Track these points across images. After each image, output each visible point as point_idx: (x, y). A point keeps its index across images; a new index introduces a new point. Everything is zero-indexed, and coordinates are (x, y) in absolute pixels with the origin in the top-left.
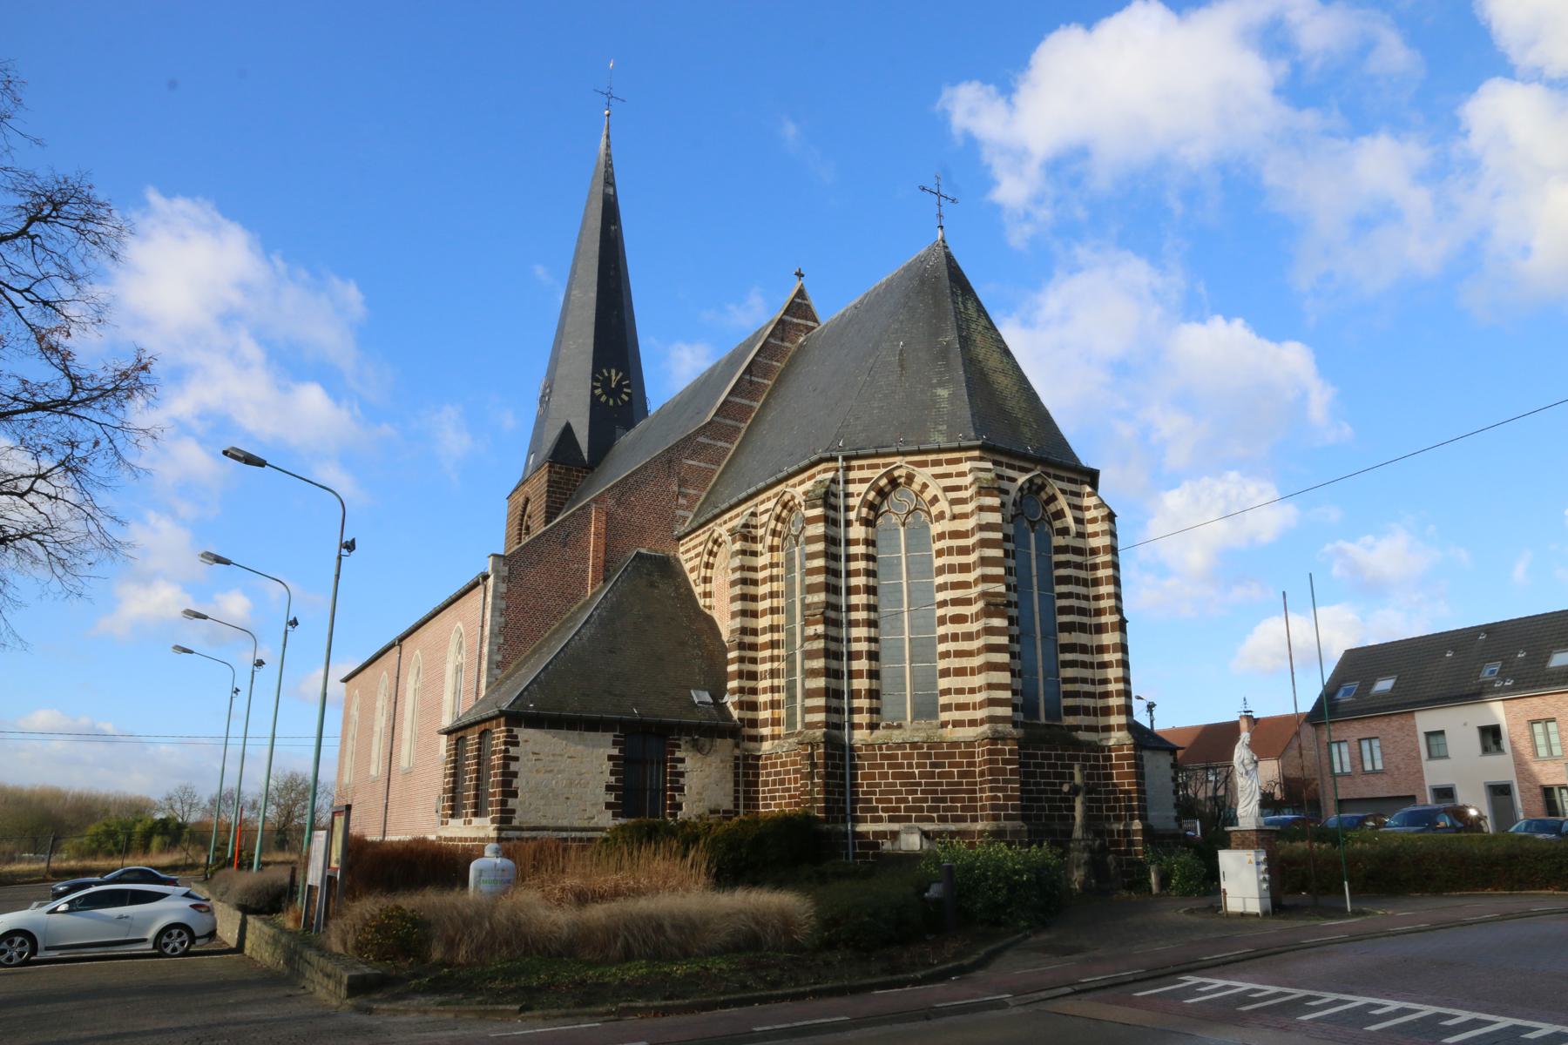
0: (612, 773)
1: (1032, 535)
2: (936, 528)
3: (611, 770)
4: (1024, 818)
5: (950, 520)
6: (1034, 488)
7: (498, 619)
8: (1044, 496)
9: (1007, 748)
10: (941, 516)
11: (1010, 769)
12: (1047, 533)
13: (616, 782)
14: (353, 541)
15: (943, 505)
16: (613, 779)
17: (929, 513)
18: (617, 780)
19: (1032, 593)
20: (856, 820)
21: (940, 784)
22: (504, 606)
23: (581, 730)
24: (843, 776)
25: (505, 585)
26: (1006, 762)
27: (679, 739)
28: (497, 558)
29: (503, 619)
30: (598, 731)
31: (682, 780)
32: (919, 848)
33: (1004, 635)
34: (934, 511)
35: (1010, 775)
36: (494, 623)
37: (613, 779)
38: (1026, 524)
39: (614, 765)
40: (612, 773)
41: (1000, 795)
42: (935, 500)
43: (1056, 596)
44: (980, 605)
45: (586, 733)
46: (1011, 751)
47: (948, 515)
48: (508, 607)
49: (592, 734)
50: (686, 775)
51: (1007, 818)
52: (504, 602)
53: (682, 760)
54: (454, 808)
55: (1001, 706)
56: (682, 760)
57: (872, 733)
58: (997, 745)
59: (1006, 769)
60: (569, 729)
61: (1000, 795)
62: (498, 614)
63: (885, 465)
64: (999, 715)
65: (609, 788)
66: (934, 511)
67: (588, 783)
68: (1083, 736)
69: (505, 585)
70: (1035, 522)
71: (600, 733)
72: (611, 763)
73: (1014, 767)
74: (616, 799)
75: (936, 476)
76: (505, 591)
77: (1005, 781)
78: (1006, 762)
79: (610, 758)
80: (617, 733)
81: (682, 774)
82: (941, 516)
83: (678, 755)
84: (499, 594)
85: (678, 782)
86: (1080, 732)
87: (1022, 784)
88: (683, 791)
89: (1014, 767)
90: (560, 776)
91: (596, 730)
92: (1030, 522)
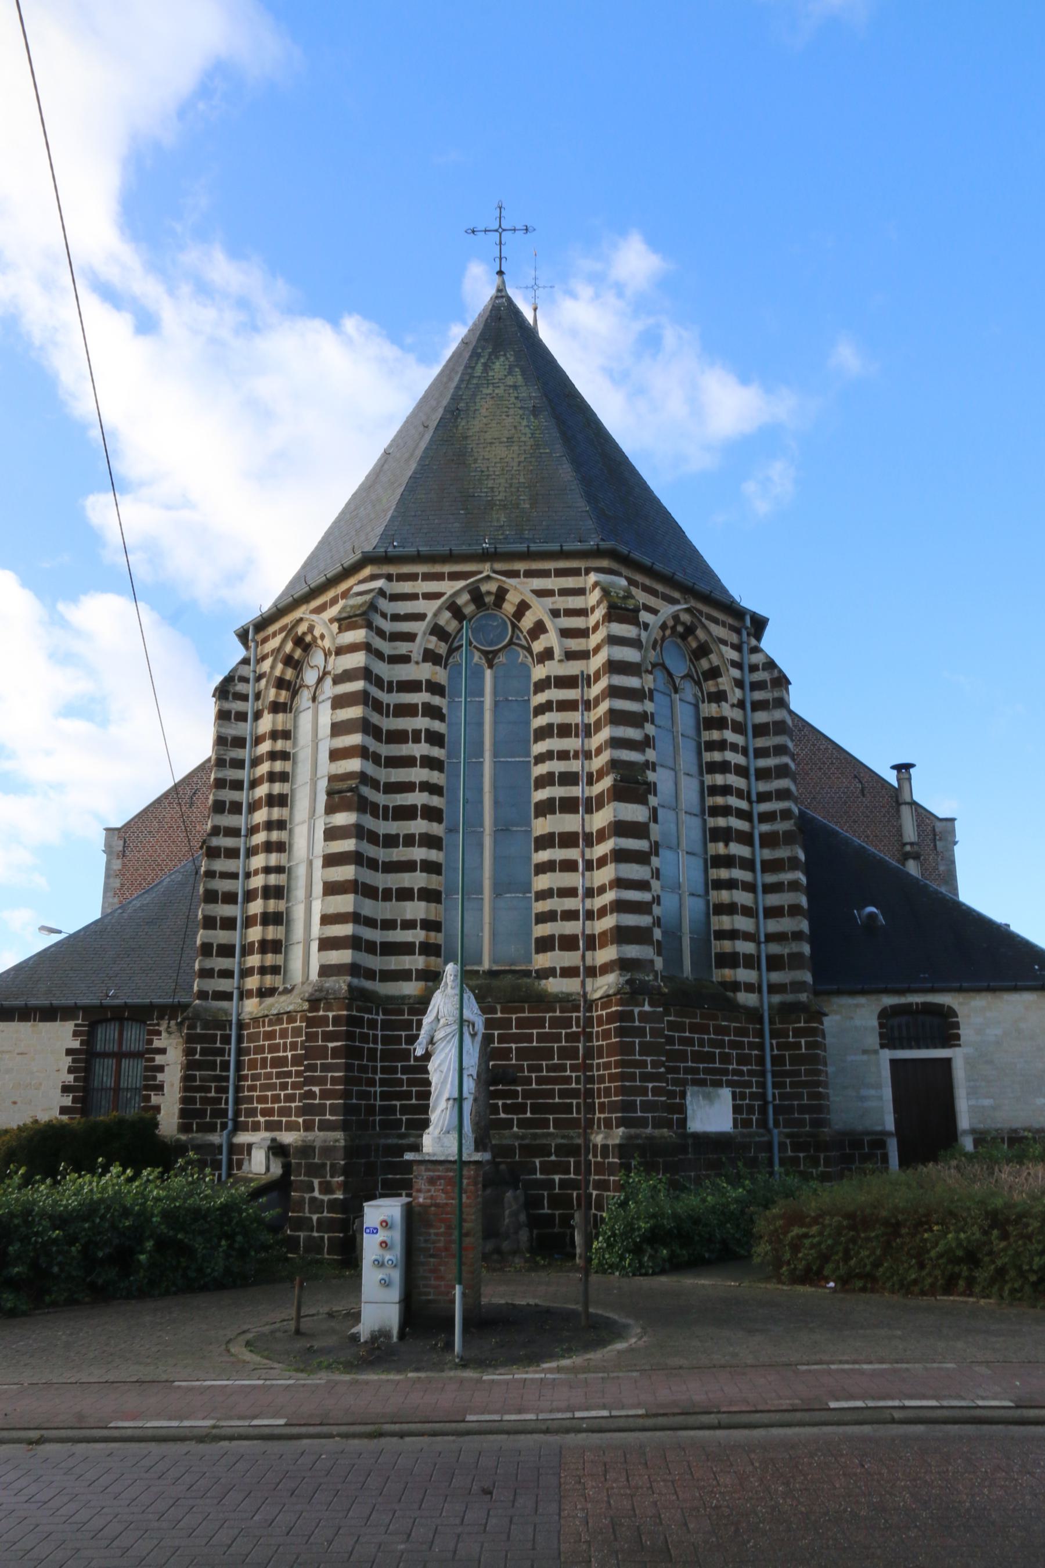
0: (70, 1071)
1: (488, 673)
2: (539, 672)
3: (70, 1067)
4: (345, 1126)
5: (560, 661)
6: (489, 600)
7: (111, 900)
8: (509, 608)
9: (331, 1014)
10: (547, 655)
11: (333, 1049)
12: (523, 664)
13: (74, 1082)
14: (894, 767)
15: (551, 639)
16: (71, 1077)
17: (529, 650)
18: (76, 1079)
19: (482, 763)
20: (238, 1127)
21: (644, 1091)
22: (118, 885)
23: (35, 1020)
24: (225, 1066)
25: (119, 861)
26: (328, 1037)
27: (158, 1025)
28: (111, 832)
29: (116, 900)
30: (13, 1021)
31: (160, 1076)
32: (263, 1170)
33: (350, 838)
34: (538, 647)
35: (332, 1058)
36: (106, 905)
37: (71, 1077)
38: (477, 657)
39: (74, 1061)
40: (70, 1071)
41: (316, 1089)
42: (539, 629)
43: (533, 761)
44: (606, 783)
45: (41, 1024)
46: (337, 1020)
47: (557, 653)
48: (122, 885)
49: (48, 1024)
50: (166, 1069)
51: (325, 1126)
52: (118, 881)
53: (163, 1051)
54: (477, 1149)
55: (337, 949)
56: (163, 1051)
57: (261, 1003)
58: (318, 1010)
59: (327, 1047)
60: (20, 1020)
61: (316, 1089)
62: (111, 894)
63: (281, 630)
64: (333, 962)
65: (66, 1089)
66: (538, 647)
67: (41, 1084)
68: (555, 985)
69: (119, 861)
70: (495, 653)
71: (58, 1023)
72: (70, 1058)
73: (339, 1044)
74: (73, 1102)
75: (541, 593)
76: (120, 867)
77: (326, 1068)
78: (328, 1037)
79: (69, 1052)
80: (80, 1022)
81: (161, 1069)
82: (547, 655)
83: (157, 1043)
84: (112, 872)
85: (155, 1078)
86: (551, 979)
87: (348, 1068)
88: (163, 1091)
89: (339, 1044)
90: (7, 1076)
91: (53, 1019)
92: (485, 653)
